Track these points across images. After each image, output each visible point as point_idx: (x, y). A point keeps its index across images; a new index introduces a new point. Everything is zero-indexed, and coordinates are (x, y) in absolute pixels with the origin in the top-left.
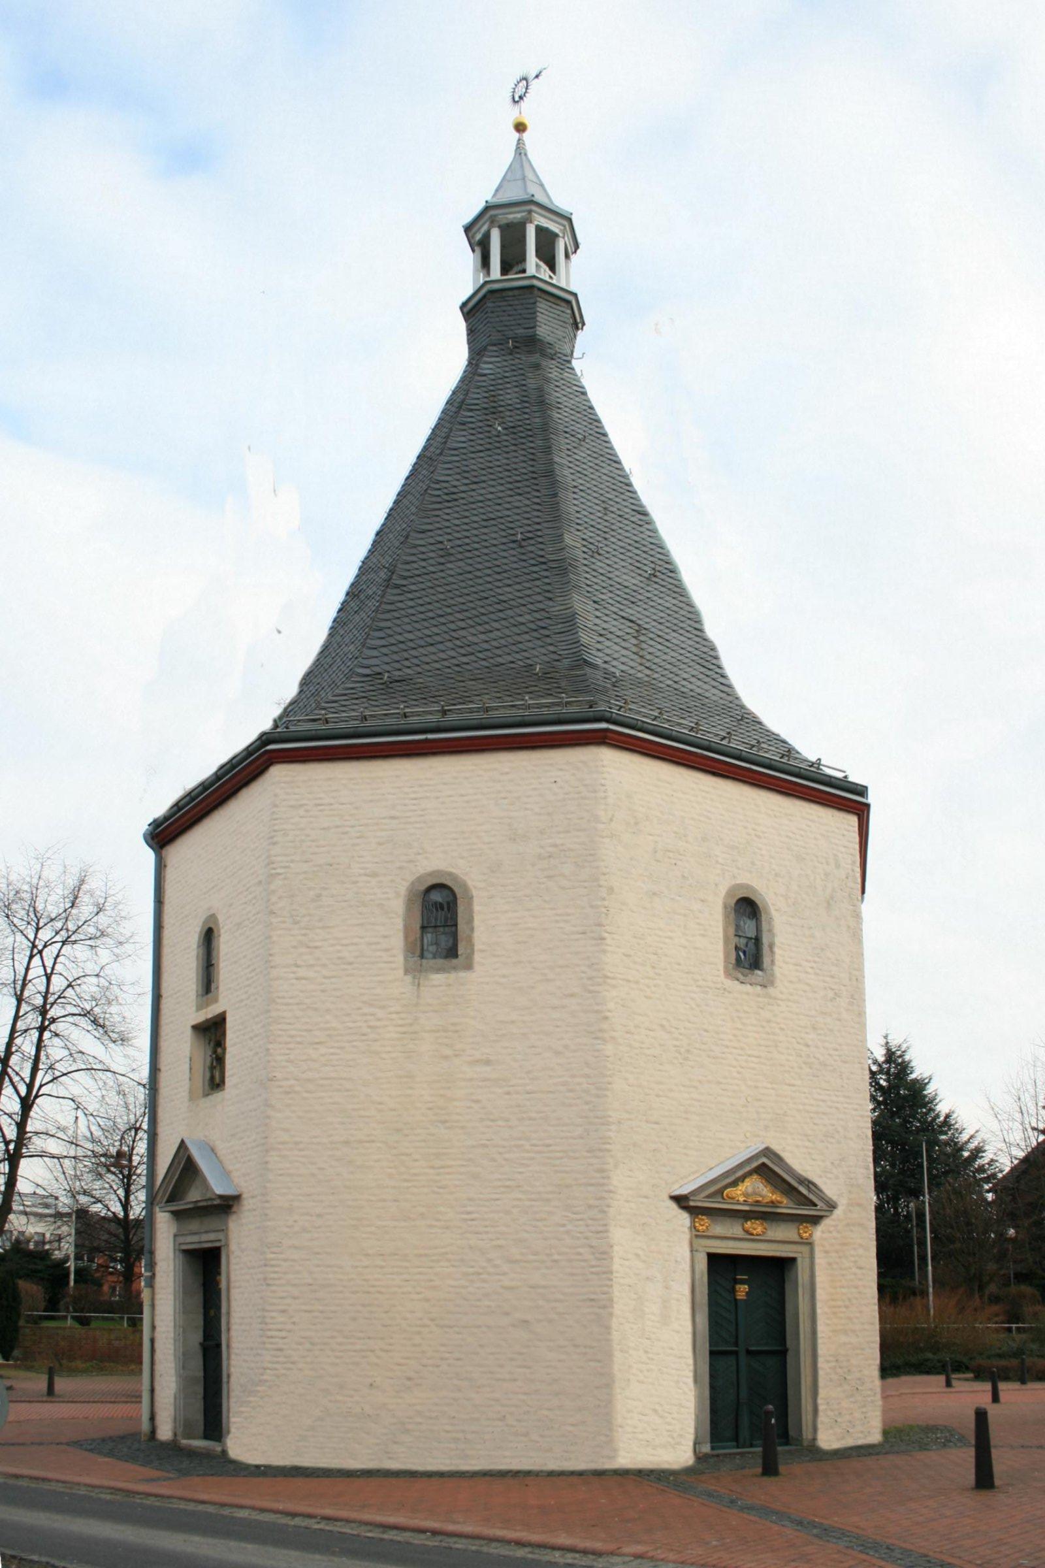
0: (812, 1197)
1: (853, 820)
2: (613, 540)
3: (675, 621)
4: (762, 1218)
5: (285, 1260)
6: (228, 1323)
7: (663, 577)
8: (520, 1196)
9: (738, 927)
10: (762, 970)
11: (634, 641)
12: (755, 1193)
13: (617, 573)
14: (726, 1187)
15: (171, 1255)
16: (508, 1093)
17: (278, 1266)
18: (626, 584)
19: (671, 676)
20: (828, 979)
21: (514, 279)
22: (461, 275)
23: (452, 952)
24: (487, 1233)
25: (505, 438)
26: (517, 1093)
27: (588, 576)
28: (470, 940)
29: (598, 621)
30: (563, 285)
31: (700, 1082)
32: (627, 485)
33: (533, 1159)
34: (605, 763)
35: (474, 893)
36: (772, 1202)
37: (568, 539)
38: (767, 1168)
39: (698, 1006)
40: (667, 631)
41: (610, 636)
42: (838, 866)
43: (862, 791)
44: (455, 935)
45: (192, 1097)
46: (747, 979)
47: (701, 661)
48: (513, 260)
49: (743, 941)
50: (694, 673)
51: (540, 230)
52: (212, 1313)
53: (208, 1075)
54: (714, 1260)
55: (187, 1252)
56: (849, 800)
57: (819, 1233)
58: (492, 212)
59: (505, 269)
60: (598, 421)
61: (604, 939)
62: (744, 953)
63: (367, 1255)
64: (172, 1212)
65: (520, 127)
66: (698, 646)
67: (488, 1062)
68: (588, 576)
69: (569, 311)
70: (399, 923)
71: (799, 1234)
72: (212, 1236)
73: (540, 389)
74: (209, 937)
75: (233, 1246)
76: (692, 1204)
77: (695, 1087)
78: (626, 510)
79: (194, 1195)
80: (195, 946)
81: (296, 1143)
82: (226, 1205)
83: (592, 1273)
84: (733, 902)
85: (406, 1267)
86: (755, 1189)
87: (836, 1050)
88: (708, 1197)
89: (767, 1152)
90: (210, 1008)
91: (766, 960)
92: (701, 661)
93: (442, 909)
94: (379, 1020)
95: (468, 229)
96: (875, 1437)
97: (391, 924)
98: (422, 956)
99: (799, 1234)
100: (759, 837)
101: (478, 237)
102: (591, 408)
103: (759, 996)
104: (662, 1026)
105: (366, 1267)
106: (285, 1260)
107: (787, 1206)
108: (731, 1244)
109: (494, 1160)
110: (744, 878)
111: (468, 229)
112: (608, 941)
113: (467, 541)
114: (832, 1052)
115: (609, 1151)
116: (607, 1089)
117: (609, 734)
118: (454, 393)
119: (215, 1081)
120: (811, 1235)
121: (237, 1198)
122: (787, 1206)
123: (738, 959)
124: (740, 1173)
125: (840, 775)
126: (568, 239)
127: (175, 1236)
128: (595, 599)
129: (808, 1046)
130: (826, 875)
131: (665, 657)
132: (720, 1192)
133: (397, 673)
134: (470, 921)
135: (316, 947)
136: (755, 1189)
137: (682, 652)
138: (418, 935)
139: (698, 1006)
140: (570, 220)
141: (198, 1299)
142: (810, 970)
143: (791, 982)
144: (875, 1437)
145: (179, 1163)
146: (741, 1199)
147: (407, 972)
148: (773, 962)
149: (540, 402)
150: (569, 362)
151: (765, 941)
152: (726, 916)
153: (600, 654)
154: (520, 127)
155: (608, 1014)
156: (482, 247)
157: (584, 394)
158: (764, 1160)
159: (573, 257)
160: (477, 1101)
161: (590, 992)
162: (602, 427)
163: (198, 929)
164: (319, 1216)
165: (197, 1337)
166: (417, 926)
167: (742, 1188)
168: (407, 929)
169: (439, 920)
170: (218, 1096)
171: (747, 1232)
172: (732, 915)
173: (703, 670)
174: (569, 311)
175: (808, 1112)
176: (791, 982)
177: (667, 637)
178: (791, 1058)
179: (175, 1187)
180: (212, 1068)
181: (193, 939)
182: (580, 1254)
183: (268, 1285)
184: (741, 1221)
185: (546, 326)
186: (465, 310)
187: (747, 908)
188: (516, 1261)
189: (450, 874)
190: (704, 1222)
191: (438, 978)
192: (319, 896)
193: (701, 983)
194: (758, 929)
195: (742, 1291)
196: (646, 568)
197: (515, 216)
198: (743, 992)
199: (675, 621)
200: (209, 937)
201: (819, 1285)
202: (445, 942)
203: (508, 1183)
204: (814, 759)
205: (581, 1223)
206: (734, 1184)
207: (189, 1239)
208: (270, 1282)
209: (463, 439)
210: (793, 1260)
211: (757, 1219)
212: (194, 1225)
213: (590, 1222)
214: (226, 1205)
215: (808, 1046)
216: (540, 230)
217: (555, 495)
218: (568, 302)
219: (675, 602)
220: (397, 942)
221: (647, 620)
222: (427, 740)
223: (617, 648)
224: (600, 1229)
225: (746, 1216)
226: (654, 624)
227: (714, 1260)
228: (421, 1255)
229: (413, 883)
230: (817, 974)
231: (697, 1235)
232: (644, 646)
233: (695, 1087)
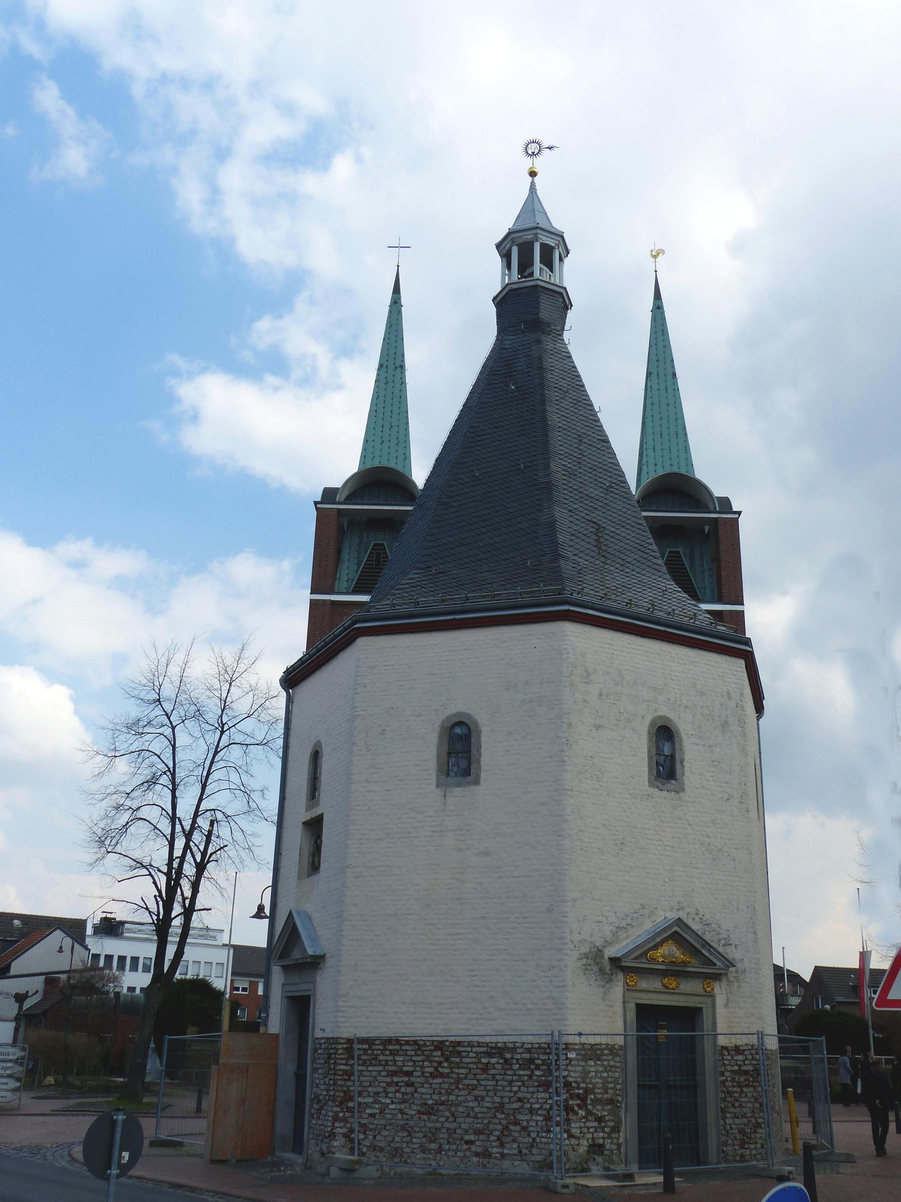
0: (712, 958)
2: (585, 463)
3: (624, 520)
5: (350, 1007)
7: (616, 487)
9: (658, 747)
10: (675, 780)
11: (595, 537)
12: (670, 955)
13: (586, 487)
15: (280, 1000)
16: (501, 877)
18: (591, 495)
19: (619, 560)
20: (723, 785)
22: (492, 276)
23: (466, 772)
24: (484, 986)
25: (516, 394)
27: (566, 492)
28: (478, 761)
29: (571, 525)
30: (557, 282)
32: (596, 421)
34: (568, 633)
36: (683, 962)
37: (553, 467)
40: (618, 527)
41: (579, 535)
42: (730, 698)
44: (469, 759)
45: (300, 878)
46: (669, 786)
47: (640, 548)
48: (525, 266)
49: (662, 758)
50: (636, 557)
51: (543, 246)
55: (290, 998)
58: (513, 236)
60: (579, 376)
61: (564, 762)
63: (404, 1003)
64: (282, 966)
65: (533, 174)
66: (639, 536)
68: (566, 492)
70: (434, 751)
73: (540, 358)
74: (316, 756)
75: (318, 996)
76: (624, 964)
78: (594, 440)
79: (296, 955)
82: (315, 963)
86: (670, 950)
87: (730, 840)
88: (635, 958)
89: (679, 922)
90: (314, 810)
92: (640, 548)
95: (498, 246)
97: (427, 750)
98: (448, 775)
102: (575, 367)
103: (673, 799)
104: (604, 825)
106: (350, 1007)
108: (653, 996)
110: (664, 711)
111: (498, 246)
113: (489, 469)
114: (727, 841)
118: (487, 359)
119: (314, 866)
120: (713, 989)
121: (322, 957)
123: (658, 772)
124: (658, 940)
126: (562, 249)
127: (283, 985)
128: (570, 509)
129: (708, 837)
130: (722, 704)
131: (615, 547)
132: (645, 954)
133: (441, 566)
134: (479, 749)
136: (670, 950)
137: (628, 542)
138: (446, 759)
140: (563, 237)
142: (711, 779)
143: (696, 788)
147: (438, 786)
148: (683, 773)
149: (539, 368)
150: (561, 335)
151: (677, 758)
152: (650, 740)
153: (571, 549)
154: (533, 174)
156: (506, 257)
157: (570, 357)
158: (677, 929)
159: (566, 260)
160: (480, 883)
162: (581, 381)
163: (310, 751)
164: (374, 972)
166: (445, 754)
168: (438, 756)
169: (459, 750)
170: (315, 878)
171: (665, 986)
172: (654, 740)
173: (642, 554)
174: (561, 302)
176: (696, 788)
177: (618, 532)
178: (697, 847)
179: (285, 946)
181: (306, 758)
185: (545, 314)
187: (664, 733)
189: (467, 714)
190: (633, 979)
191: (457, 791)
192: (384, 730)
194: (674, 750)
196: (605, 482)
197: (529, 236)
198: (663, 798)
199: (624, 520)
200: (316, 756)
202: (463, 764)
203: (499, 947)
206: (656, 947)
207: (291, 988)
209: (490, 396)
211: (672, 976)
214: (315, 963)
215: (708, 837)
216: (543, 246)
217: (546, 435)
218: (561, 294)
219: (625, 505)
220: (432, 765)
221: (605, 520)
223: (583, 543)
224: (560, 984)
225: (664, 974)
226: (609, 523)
229: (443, 722)
230: (715, 781)
231: (628, 989)
232: (602, 540)
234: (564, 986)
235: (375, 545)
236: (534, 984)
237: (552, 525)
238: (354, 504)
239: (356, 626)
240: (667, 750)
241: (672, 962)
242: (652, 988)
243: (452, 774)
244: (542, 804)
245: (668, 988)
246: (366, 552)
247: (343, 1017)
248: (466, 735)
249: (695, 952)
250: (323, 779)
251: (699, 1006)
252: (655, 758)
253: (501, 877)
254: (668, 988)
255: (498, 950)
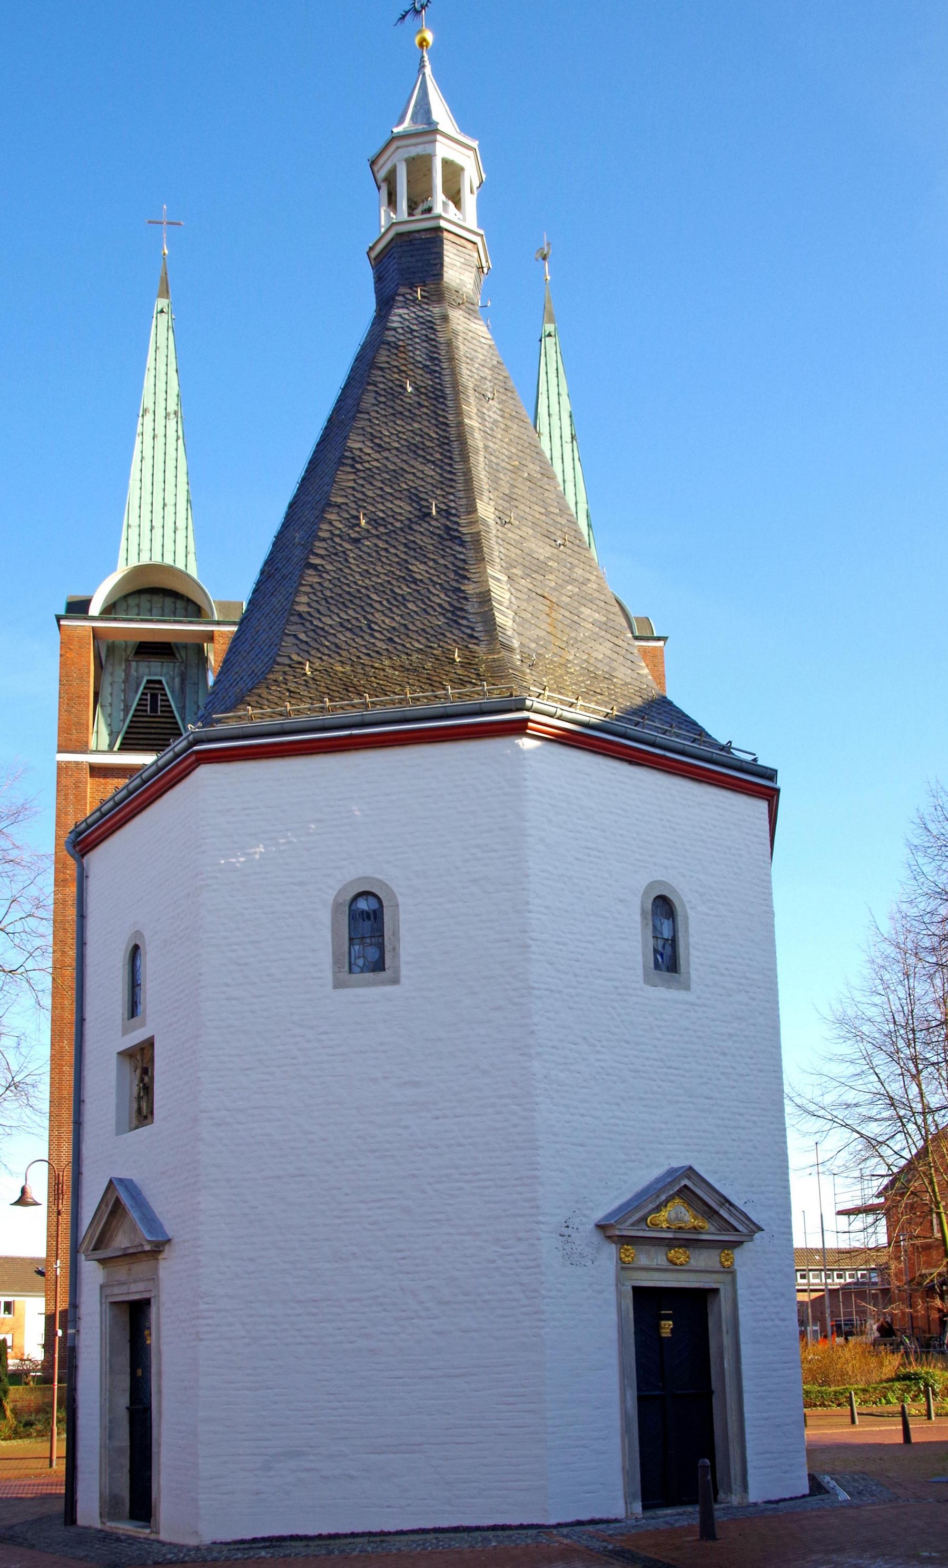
1: (763, 806)
4: (685, 1246)
6: (159, 1386)
8: (451, 1231)
12: (678, 1219)
14: (650, 1213)
17: (212, 1317)
20: (743, 981)
21: (421, 224)
23: (379, 966)
26: (445, 1117)
31: (622, 1098)
33: (460, 1189)
35: (400, 900)
36: (695, 1228)
37: (480, 505)
38: (686, 1187)
39: (619, 1015)
43: (771, 775)
44: (381, 947)
45: (119, 1131)
49: (660, 942)
51: (446, 163)
52: (139, 1372)
53: (135, 1106)
54: (640, 1293)
56: (758, 784)
57: (742, 1259)
59: (412, 208)
62: (662, 955)
64: (99, 1261)
67: (416, 1084)
69: (476, 255)
71: (721, 1262)
72: (141, 1286)
73: (449, 344)
74: (135, 951)
75: (164, 1298)
77: (618, 1104)
79: (121, 1241)
80: (121, 965)
81: (228, 1180)
83: (523, 1313)
84: (649, 906)
85: (339, 1314)
86: (676, 1214)
87: (752, 1058)
88: (632, 1225)
89: (690, 1171)
91: (682, 962)
93: (369, 918)
94: (309, 1041)
96: (807, 1491)
99: (721, 1262)
100: (675, 830)
101: (382, 174)
104: (585, 1039)
105: (299, 1315)
107: (710, 1232)
108: (656, 1275)
109: (423, 1191)
112: (533, 949)
115: (536, 1177)
116: (533, 1110)
117: (530, 724)
119: (143, 1112)
122: (710, 1232)
125: (749, 758)
135: (247, 964)
136: (676, 1214)
139: (619, 1015)
141: (124, 1360)
142: (725, 972)
143: (706, 985)
144: (807, 1491)
145: (107, 1206)
146: (664, 1225)
155: (535, 1028)
158: (686, 1182)
160: (407, 1127)
161: (516, 1004)
163: (123, 947)
164: (251, 1260)
165: (124, 1400)
167: (664, 1214)
169: (366, 930)
171: (671, 1262)
175: (726, 1127)
176: (706, 985)
180: (139, 1098)
182: (509, 1292)
183: (201, 1340)
184: (665, 1249)
186: (373, 255)
187: (663, 907)
188: (448, 1303)
193: (622, 990)
195: (667, 1327)
198: (663, 995)
200: (135, 951)
201: (742, 1319)
202: (372, 953)
203: (438, 1216)
204: (723, 741)
205: (510, 1257)
208: (204, 1337)
210: (716, 1291)
211: (680, 1247)
212: (121, 1272)
213: (520, 1257)
214: (157, 1249)
220: (326, 957)
222: (351, 736)
225: (670, 1244)
227: (640, 1293)
228: (353, 1300)
230: (732, 976)
231: (624, 1267)
233: (618, 1104)
234: (538, 1266)
235: (149, 682)
236: (494, 1265)
237: (485, 598)
238: (115, 620)
239: (195, 748)
240: (667, 934)
241: (680, 1228)
242: (654, 1264)
243: (355, 968)
244: (498, 1008)
245: (676, 1264)
246: (136, 692)
247: (208, 1325)
248: (375, 912)
249: (710, 1213)
250: (148, 986)
251: (714, 1286)
252: (651, 941)
253: (437, 1118)
254: (676, 1264)
255: (436, 1221)
